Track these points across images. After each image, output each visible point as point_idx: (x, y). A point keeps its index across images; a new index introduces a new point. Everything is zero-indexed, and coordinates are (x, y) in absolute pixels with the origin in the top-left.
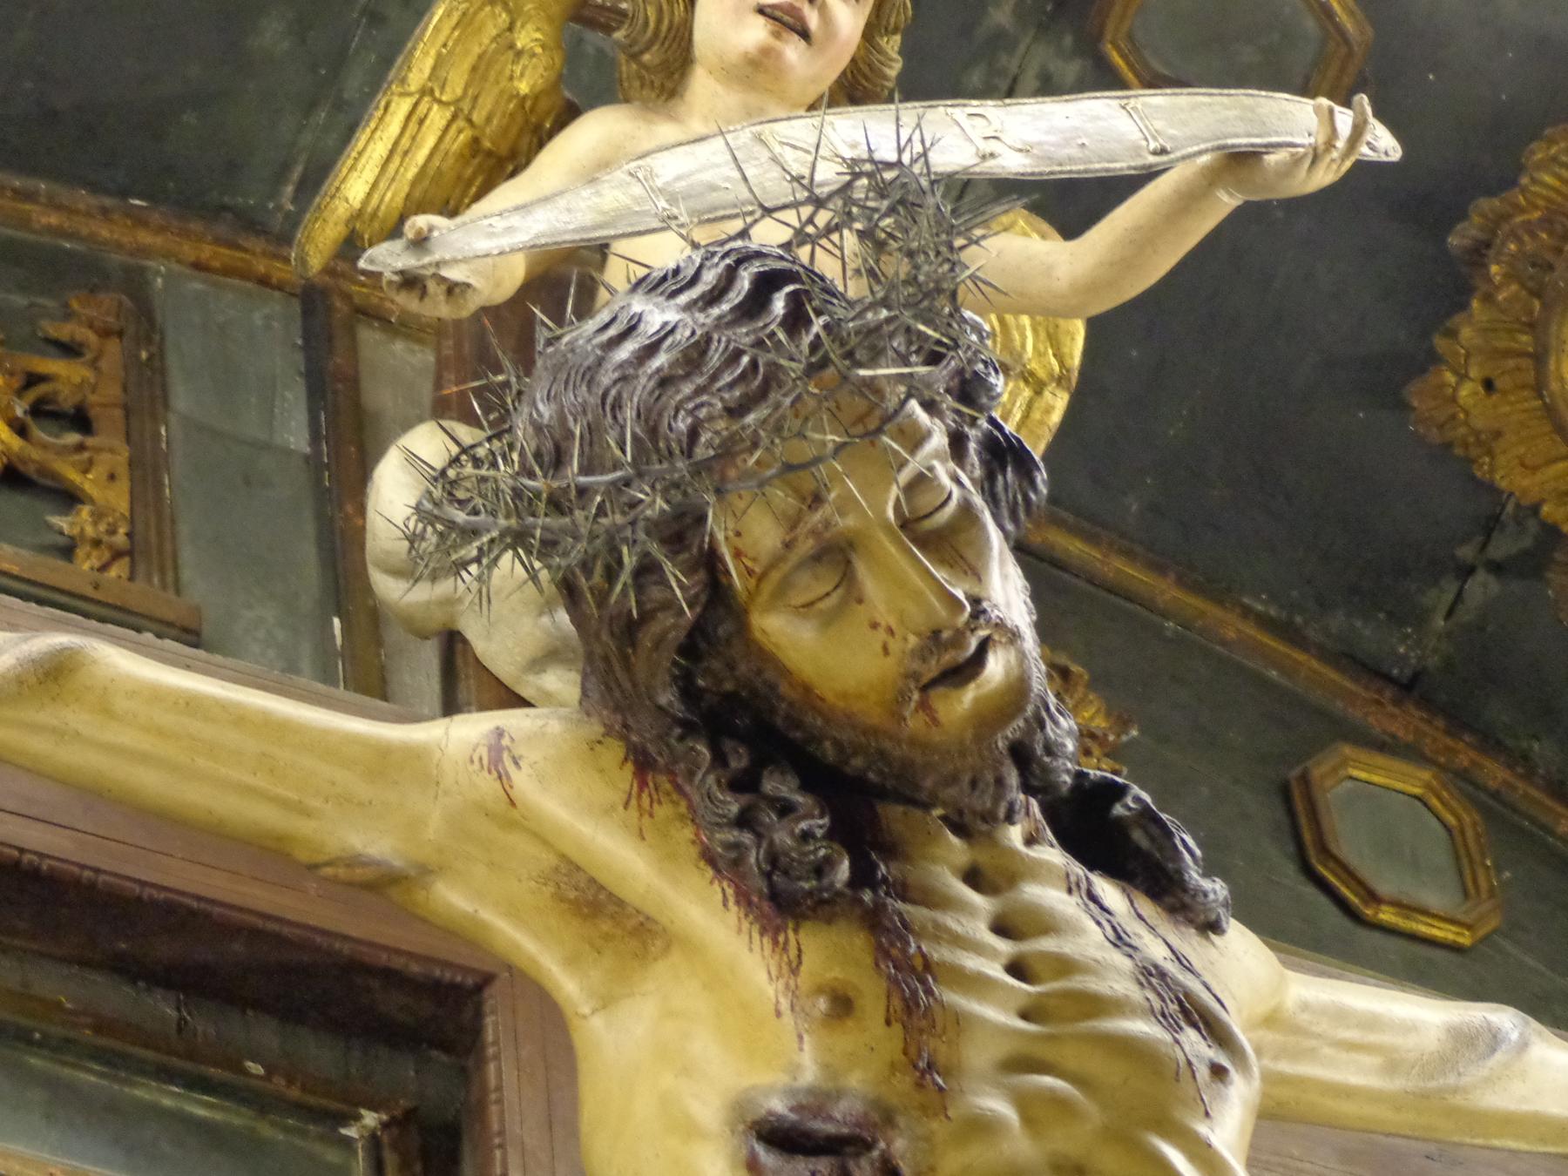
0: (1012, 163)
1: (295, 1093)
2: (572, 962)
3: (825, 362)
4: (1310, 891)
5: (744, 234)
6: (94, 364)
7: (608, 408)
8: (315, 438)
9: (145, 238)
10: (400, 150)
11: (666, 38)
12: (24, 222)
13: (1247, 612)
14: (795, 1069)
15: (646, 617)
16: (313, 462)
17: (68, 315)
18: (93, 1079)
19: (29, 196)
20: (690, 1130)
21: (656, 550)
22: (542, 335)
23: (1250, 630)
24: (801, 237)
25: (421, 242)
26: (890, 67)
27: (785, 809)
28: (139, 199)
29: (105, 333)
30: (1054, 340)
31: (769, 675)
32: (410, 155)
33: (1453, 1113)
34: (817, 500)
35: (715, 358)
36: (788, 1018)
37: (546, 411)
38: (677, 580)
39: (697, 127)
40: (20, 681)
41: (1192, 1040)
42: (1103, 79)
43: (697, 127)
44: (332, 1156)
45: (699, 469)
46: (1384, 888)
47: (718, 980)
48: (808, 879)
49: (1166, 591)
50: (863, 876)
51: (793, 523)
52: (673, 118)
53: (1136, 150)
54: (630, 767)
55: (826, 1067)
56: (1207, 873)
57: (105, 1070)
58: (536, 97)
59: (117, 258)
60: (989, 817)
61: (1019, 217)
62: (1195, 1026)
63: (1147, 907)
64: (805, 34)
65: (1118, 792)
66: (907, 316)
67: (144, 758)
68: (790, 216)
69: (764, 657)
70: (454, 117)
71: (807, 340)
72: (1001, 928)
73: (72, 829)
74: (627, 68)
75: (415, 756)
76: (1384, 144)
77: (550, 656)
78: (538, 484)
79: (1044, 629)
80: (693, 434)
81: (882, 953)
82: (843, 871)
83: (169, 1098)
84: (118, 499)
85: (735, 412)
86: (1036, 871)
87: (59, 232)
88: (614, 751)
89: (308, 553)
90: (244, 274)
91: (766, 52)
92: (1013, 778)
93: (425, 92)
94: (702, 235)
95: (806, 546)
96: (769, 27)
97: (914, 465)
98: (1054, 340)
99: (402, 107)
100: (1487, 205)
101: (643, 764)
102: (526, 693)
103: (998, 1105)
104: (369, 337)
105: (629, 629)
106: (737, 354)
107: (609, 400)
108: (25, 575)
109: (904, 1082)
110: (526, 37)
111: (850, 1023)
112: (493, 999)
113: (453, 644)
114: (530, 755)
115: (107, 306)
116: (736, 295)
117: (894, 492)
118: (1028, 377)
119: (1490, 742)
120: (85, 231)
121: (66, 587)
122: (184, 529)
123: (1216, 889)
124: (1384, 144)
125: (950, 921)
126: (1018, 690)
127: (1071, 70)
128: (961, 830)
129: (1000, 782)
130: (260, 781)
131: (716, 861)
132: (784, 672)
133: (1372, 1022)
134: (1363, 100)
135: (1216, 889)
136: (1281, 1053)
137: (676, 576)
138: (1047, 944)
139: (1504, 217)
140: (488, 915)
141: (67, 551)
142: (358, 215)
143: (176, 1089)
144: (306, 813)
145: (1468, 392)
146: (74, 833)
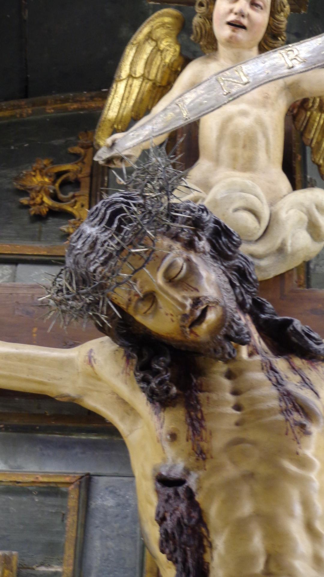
2: (122, 419)
3: (123, 249)
10: (125, 98)
11: (205, 35)
12: (66, 110)
19: (66, 100)
26: (281, 24)
28: (105, 89)
32: (129, 98)
51: (129, 293)
52: (216, 59)
54: (125, 358)
62: (297, 411)
64: (244, 27)
70: (143, 80)
91: (231, 37)
96: (231, 29)
108: (49, 254)
111: (176, 443)
120: (86, 106)
130: (31, 377)
137: (103, 317)
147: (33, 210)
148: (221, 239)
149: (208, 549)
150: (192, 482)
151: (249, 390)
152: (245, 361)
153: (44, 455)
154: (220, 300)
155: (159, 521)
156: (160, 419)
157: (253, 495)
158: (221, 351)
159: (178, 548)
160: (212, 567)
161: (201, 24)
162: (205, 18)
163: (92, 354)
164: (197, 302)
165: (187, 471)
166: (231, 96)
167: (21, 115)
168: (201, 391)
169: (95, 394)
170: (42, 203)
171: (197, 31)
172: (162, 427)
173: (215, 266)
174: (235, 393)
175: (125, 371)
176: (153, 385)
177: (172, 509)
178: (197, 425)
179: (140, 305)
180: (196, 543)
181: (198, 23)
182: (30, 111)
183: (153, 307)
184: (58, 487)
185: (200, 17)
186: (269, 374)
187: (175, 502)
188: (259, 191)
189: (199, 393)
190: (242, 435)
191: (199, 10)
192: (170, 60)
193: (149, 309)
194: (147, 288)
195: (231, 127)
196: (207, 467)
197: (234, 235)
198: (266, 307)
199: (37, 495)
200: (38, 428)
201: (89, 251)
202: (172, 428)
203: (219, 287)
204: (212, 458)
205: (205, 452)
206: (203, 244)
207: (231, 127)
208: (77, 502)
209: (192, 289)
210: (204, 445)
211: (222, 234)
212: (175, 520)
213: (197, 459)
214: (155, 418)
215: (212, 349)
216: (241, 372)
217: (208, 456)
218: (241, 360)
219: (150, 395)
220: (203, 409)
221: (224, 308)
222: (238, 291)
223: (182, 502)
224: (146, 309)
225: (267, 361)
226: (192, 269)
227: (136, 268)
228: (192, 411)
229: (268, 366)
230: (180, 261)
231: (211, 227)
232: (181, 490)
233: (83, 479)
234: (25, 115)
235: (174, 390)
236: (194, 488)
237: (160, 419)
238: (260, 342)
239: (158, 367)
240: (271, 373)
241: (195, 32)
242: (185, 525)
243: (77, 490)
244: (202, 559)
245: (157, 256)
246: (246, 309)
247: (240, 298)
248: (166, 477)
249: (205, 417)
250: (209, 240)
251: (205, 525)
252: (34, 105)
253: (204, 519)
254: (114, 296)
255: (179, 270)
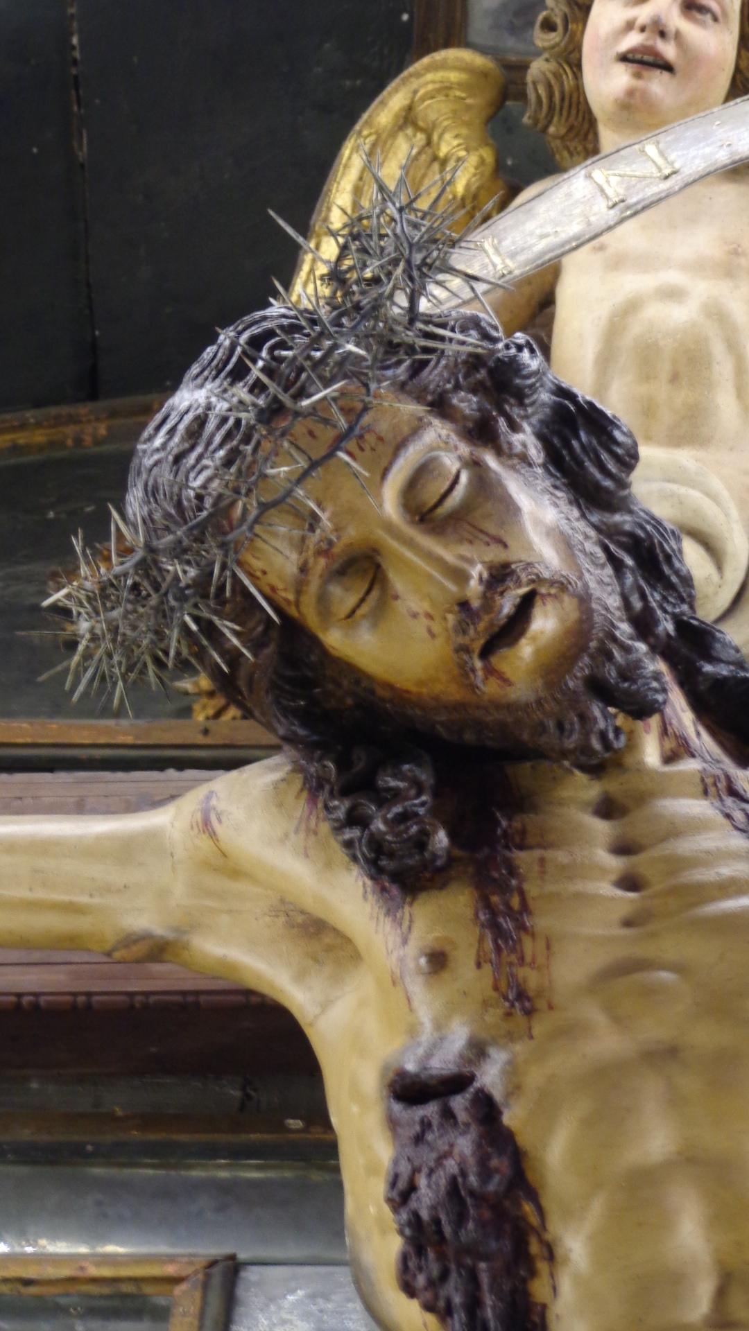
2: (300, 976)
7: (150, 494)
18: (150, 1172)
31: (365, 684)
48: (411, 856)
51: (301, 544)
54: (305, 794)
57: (155, 1161)
64: (667, 67)
73: (66, 963)
75: (152, 838)
91: (631, 93)
107: (150, 488)
108: (139, 742)
111: (446, 975)
121: (179, 741)
130: (40, 894)
137: (227, 627)
143: (223, 1161)
146: (69, 967)
148: (578, 438)
149: (542, 1266)
150: (490, 1076)
151: (664, 839)
152: (657, 772)
153: (105, 1216)
154: (573, 578)
155: (397, 1199)
156: (401, 925)
157: (675, 1101)
158: (577, 726)
159: (453, 1267)
160: (557, 1316)
161: (550, 76)
162: (562, 62)
163: (214, 802)
164: (500, 575)
165: (478, 1050)
166: (628, 208)
167: (78, 441)
168: (521, 847)
169: (225, 919)
171: (539, 97)
172: (405, 941)
173: (558, 498)
174: (623, 848)
175: (303, 827)
176: (379, 825)
177: (434, 1155)
178: (507, 924)
179: (336, 590)
180: (507, 1245)
181: (541, 71)
182: (102, 430)
183: (375, 594)
184: (144, 1297)
185: (547, 60)
186: (723, 805)
187: (441, 1136)
188: (716, 484)
189: (514, 850)
190: (646, 950)
191: (543, 40)
192: (468, 186)
193: (362, 600)
194: (352, 533)
195: (636, 328)
196: (537, 1030)
197: (618, 427)
198: (718, 640)
199: (82, 1316)
200: (89, 1148)
201: (187, 445)
202: (437, 939)
203: (566, 545)
204: (551, 1007)
205: (531, 994)
206: (526, 439)
207: (636, 328)
208: (196, 1323)
209: (487, 539)
210: (530, 978)
211: (580, 421)
212: (443, 1182)
213: (509, 1015)
214: (387, 925)
215: (551, 724)
216: (642, 798)
217: (541, 1004)
218: (641, 769)
219: (371, 855)
220: (526, 887)
221: (584, 600)
222: (629, 580)
223: (463, 1133)
224: (351, 600)
225: (719, 773)
226: (484, 484)
227: (316, 456)
228: (494, 894)
229: (722, 785)
230: (450, 463)
231: (544, 404)
232: (459, 1103)
233: (217, 1271)
234: (88, 439)
235: (441, 839)
236: (497, 1095)
237: (401, 925)
238: (698, 734)
239: (393, 783)
240: (729, 801)
241: (532, 96)
242: (472, 1193)
243: (198, 1295)
244: (526, 1294)
245: (381, 439)
246: (657, 637)
247: (637, 604)
248: (417, 1075)
249: (531, 903)
250: (540, 436)
251: (533, 1195)
252: (113, 414)
253: (530, 1176)
254: (257, 564)
255: (447, 484)
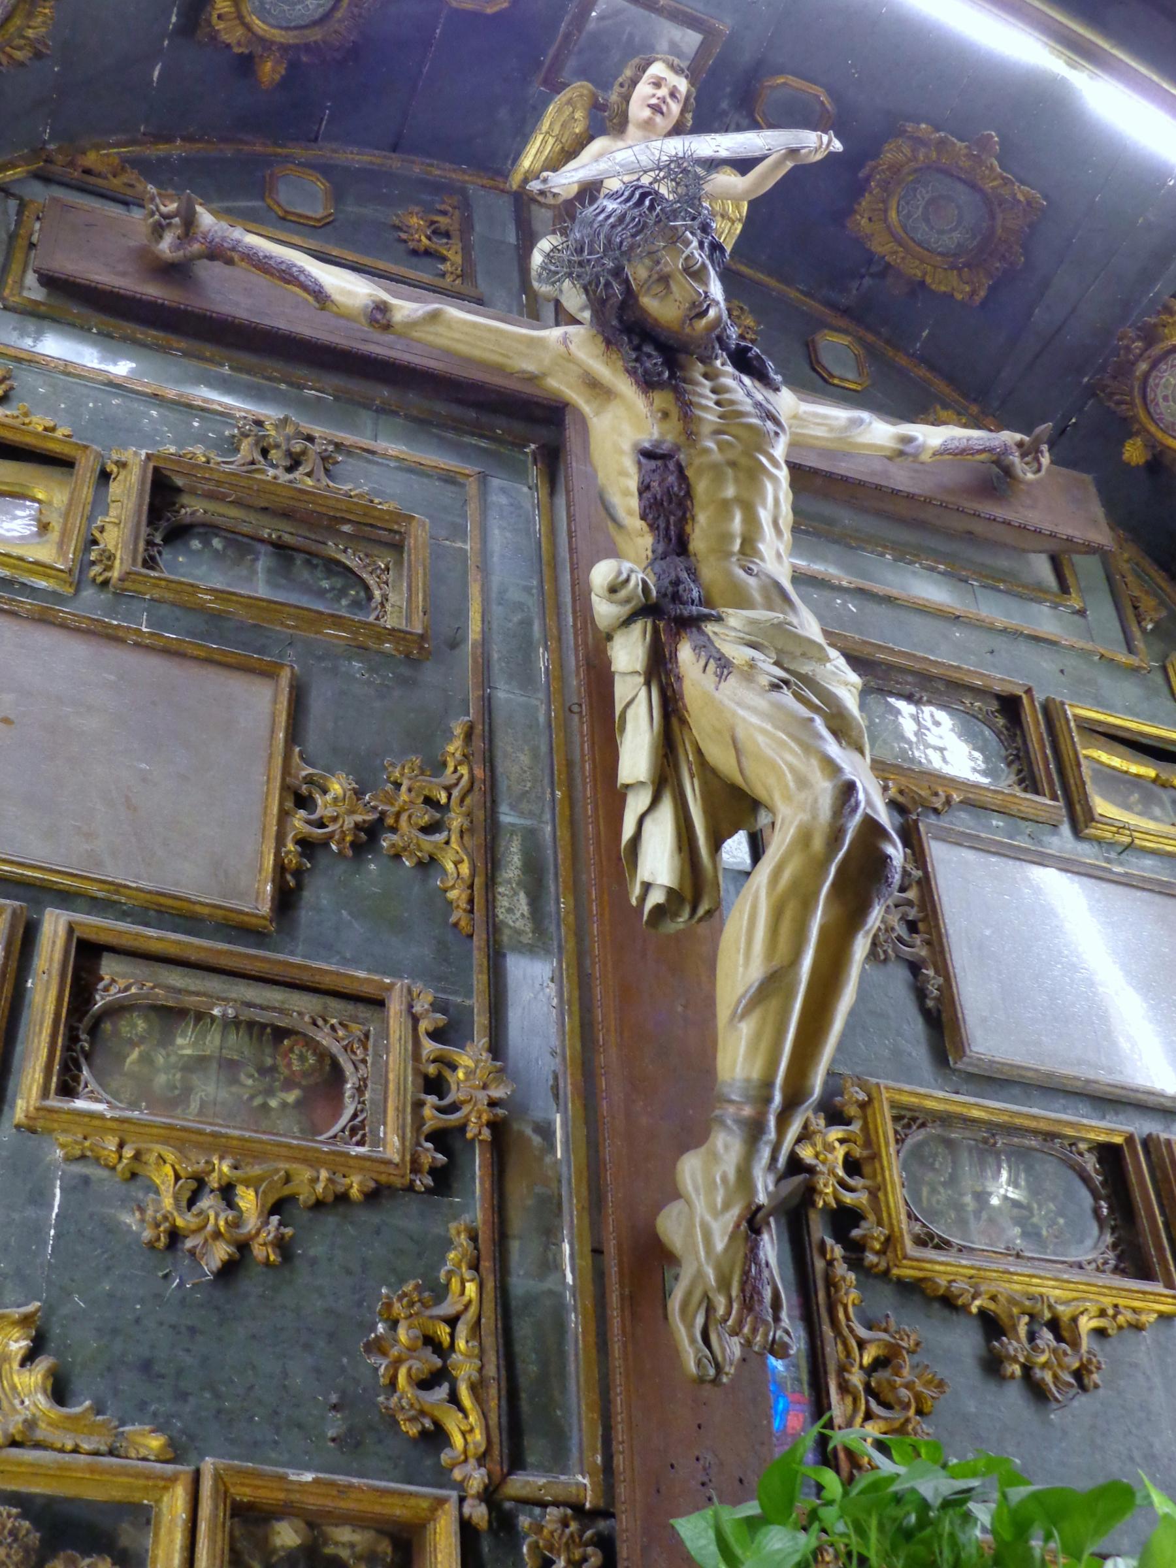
0: (724, 154)
1: (510, 439)
2: (588, 402)
3: (660, 221)
4: (814, 375)
5: (638, 179)
6: (451, 217)
8: (518, 239)
9: (467, 178)
13: (798, 290)
14: (651, 434)
15: (608, 298)
16: (517, 247)
17: (443, 202)
19: (432, 165)
20: (621, 452)
21: (610, 278)
22: (578, 211)
23: (798, 295)
24: (655, 180)
25: (545, 181)
27: (649, 356)
29: (454, 208)
30: (738, 207)
33: (850, 443)
34: (658, 263)
35: (628, 219)
36: (650, 420)
37: (578, 235)
38: (617, 288)
39: (630, 143)
40: (424, 319)
41: (770, 425)
42: (755, 126)
43: (630, 143)
44: (522, 457)
45: (623, 253)
46: (836, 372)
47: (630, 408)
49: (772, 282)
50: (672, 375)
51: (651, 270)
52: (622, 140)
53: (761, 149)
55: (661, 434)
56: (776, 373)
58: (581, 134)
59: (458, 184)
60: (710, 358)
61: (728, 169)
63: (758, 384)
64: (662, 113)
65: (751, 349)
66: (685, 206)
67: (458, 341)
68: (652, 174)
69: (643, 311)
71: (655, 214)
72: (713, 391)
74: (608, 124)
76: (837, 146)
77: (582, 309)
78: (575, 258)
79: (727, 300)
80: (621, 243)
81: (677, 399)
82: (667, 374)
83: (474, 441)
84: (458, 259)
85: (633, 236)
86: (724, 374)
87: (440, 176)
88: (600, 338)
89: (515, 275)
90: (496, 188)
92: (717, 346)
93: (547, 133)
94: (626, 179)
95: (655, 277)
97: (687, 252)
98: (738, 207)
99: (541, 137)
100: (872, 163)
101: (608, 342)
102: (579, 318)
103: (711, 444)
104: (534, 207)
105: (603, 302)
106: (634, 219)
109: (683, 438)
110: (578, 115)
112: (568, 411)
113: (558, 303)
114: (575, 340)
115: (455, 200)
116: (634, 200)
117: (681, 260)
118: (729, 219)
119: (868, 328)
122: (478, 268)
123: (778, 378)
124: (837, 146)
125: (698, 389)
126: (719, 319)
127: (745, 122)
128: (702, 362)
129: (713, 348)
131: (631, 372)
132: (649, 315)
133: (825, 417)
134: (831, 132)
135: (778, 378)
136: (798, 426)
138: (727, 396)
139: (876, 167)
140: (563, 388)
141: (443, 275)
142: (527, 171)
144: (510, 358)
145: (864, 222)
147: (411, 245)
149: (690, 522)
150: (682, 457)
157: (737, 480)
170: (420, 241)
